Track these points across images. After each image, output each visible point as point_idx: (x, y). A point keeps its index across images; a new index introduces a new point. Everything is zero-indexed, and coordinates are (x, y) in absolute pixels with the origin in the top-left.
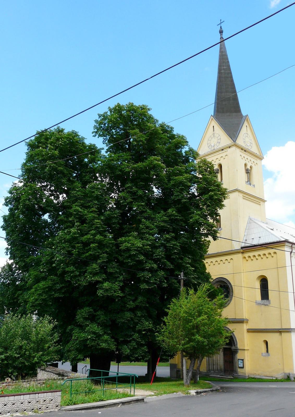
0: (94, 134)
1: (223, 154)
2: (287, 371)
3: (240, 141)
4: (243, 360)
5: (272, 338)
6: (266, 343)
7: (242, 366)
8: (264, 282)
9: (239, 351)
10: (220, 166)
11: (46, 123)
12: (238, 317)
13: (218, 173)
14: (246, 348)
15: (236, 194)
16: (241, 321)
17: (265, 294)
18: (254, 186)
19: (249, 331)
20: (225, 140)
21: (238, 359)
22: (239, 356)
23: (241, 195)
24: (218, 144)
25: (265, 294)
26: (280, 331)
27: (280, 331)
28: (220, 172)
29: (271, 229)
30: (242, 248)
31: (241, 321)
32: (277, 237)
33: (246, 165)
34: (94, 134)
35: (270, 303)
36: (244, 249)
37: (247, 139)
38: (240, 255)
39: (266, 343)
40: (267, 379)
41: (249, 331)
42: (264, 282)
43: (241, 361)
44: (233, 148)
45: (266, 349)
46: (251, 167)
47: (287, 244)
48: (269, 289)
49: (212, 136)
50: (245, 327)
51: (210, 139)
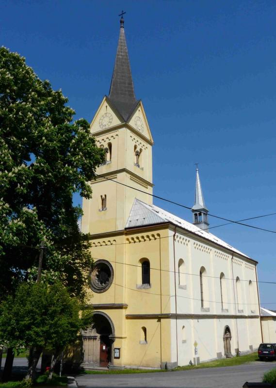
0: (104, 197)
1: (113, 134)
2: (164, 361)
3: (131, 123)
4: (119, 349)
5: (151, 324)
6: (145, 329)
7: (118, 356)
8: (146, 264)
9: (116, 339)
10: (110, 145)
11: (205, 267)
12: (118, 302)
13: (107, 152)
14: (123, 336)
15: (124, 173)
16: (120, 307)
17: (146, 279)
18: (142, 169)
19: (129, 317)
20: (117, 122)
21: (115, 349)
22: (116, 345)
23: (129, 176)
24: (109, 124)
25: (146, 279)
26: (159, 317)
27: (159, 317)
28: (109, 151)
29: (156, 212)
30: (126, 229)
31: (120, 307)
32: (161, 218)
33: (135, 147)
34: (104, 197)
35: (150, 287)
36: (127, 230)
37: (139, 123)
38: (124, 237)
39: (145, 329)
40: (145, 370)
41: (129, 317)
42: (146, 264)
43: (118, 351)
44: (124, 129)
45: (144, 337)
46: (141, 150)
47: (170, 225)
48: (151, 267)
49: (105, 116)
50: (125, 312)
51: (102, 118)
